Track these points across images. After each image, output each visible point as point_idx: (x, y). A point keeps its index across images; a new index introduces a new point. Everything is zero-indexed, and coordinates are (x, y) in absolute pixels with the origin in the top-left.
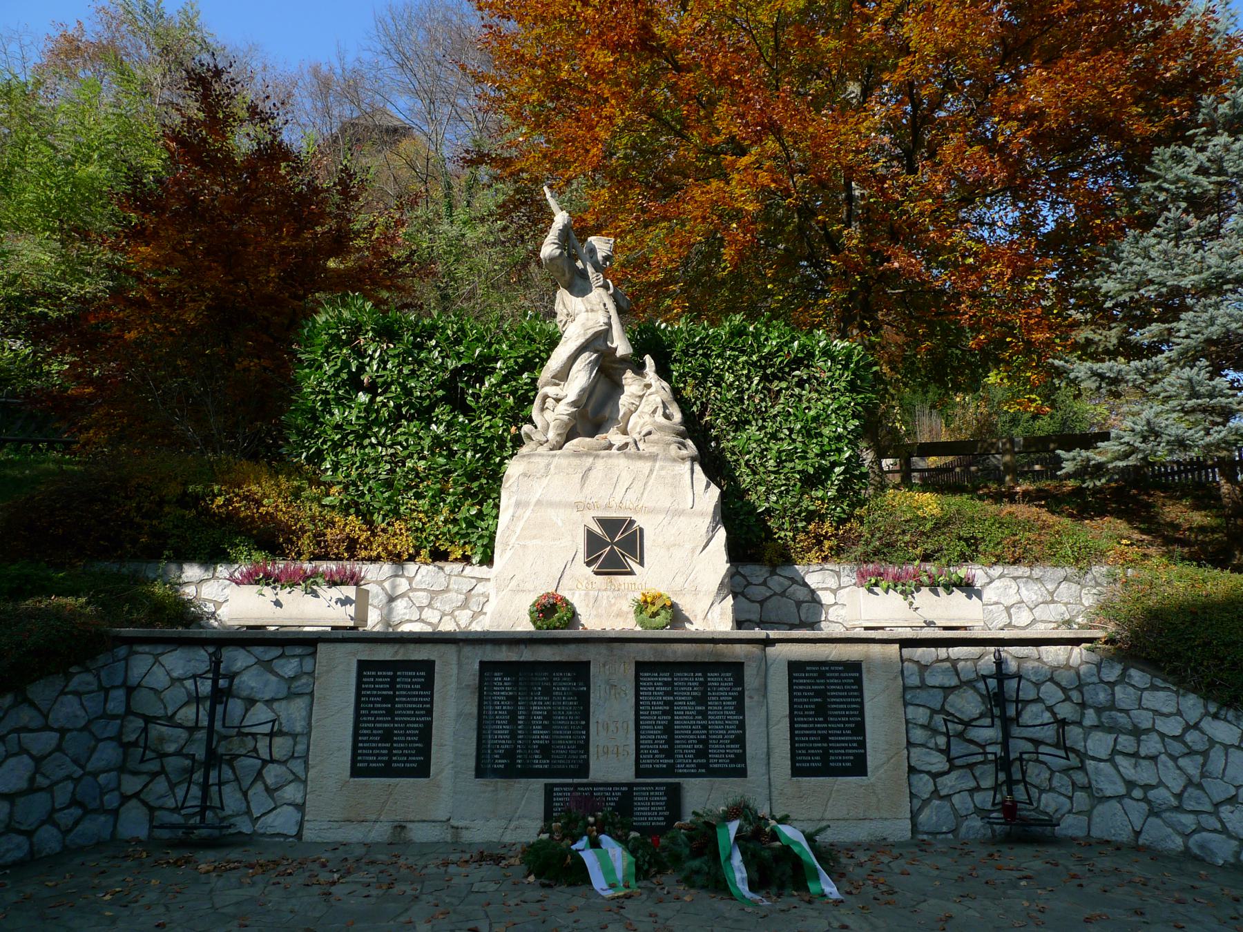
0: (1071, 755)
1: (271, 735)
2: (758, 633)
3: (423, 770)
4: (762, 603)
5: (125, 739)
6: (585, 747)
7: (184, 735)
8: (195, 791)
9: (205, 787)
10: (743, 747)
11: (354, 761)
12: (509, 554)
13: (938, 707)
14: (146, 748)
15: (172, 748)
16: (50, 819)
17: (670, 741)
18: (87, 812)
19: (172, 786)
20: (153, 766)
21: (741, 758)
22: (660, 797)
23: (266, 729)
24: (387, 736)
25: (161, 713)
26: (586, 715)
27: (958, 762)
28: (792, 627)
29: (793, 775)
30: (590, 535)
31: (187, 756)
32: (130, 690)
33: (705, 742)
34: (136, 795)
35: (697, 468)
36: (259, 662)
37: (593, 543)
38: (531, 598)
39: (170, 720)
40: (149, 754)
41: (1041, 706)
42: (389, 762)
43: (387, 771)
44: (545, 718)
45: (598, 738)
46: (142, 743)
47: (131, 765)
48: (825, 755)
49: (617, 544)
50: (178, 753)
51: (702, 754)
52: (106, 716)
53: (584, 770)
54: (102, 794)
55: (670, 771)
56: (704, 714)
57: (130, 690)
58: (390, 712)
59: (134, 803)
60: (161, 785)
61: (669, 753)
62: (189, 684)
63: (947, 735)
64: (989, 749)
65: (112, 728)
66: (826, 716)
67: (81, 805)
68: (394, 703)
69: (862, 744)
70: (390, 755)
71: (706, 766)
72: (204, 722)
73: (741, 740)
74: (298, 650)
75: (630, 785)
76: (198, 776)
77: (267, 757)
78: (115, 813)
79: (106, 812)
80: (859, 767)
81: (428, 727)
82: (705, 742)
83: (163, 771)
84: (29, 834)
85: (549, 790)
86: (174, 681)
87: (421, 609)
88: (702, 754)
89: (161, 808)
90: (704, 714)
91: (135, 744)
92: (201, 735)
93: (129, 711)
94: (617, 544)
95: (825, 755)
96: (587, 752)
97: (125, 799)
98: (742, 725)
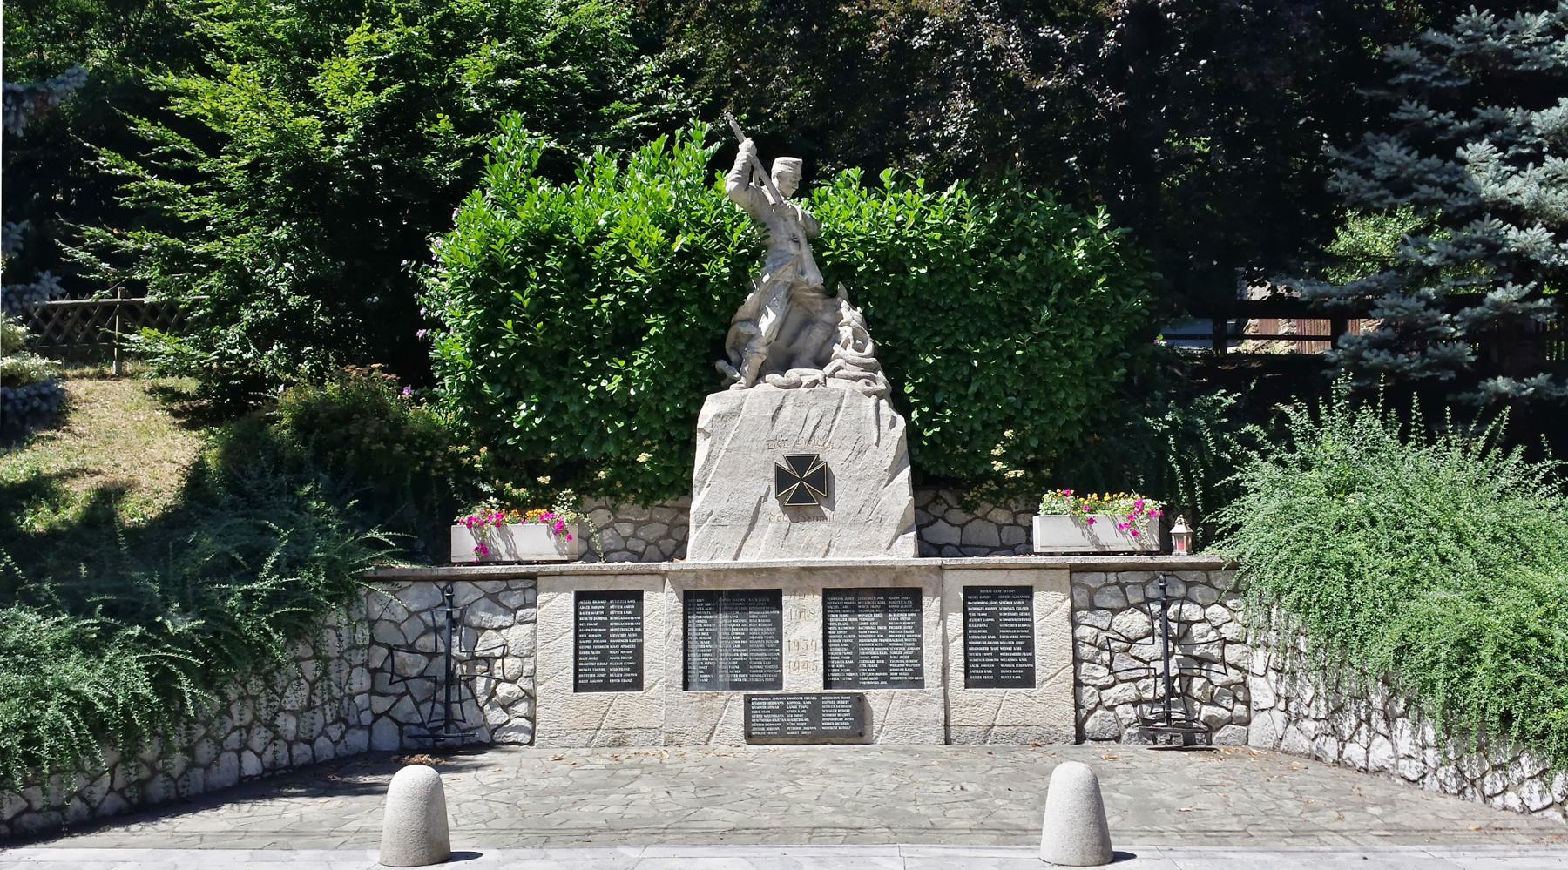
0: (1230, 670)
1: (503, 656)
2: (936, 561)
3: (637, 684)
4: (962, 526)
5: (372, 666)
6: (779, 663)
7: (424, 661)
8: (439, 708)
9: (447, 704)
10: (921, 662)
11: (576, 679)
12: (705, 491)
13: (1106, 626)
14: (393, 673)
15: (414, 672)
16: (323, 733)
17: (856, 657)
18: (349, 727)
19: (417, 704)
20: (400, 688)
21: (919, 672)
22: (846, 707)
23: (498, 652)
24: (604, 656)
25: (401, 642)
26: (779, 635)
27: (1122, 676)
28: (992, 550)
29: (967, 687)
30: (779, 470)
31: (428, 678)
32: (372, 623)
33: (886, 658)
34: (386, 713)
35: (883, 402)
36: (487, 595)
37: (782, 479)
38: (835, 470)
39: (411, 649)
40: (396, 678)
41: (1207, 626)
42: (608, 678)
43: (606, 686)
44: (743, 638)
45: (788, 657)
46: (388, 667)
47: (379, 688)
48: (997, 669)
49: (806, 480)
50: (421, 676)
51: (885, 667)
52: (354, 647)
53: (778, 683)
54: (359, 713)
55: (856, 683)
56: (886, 634)
57: (372, 623)
58: (606, 636)
59: (384, 720)
60: (407, 704)
61: (854, 668)
62: (427, 617)
63: (1111, 651)
64: (1152, 665)
65: (358, 658)
66: (998, 635)
67: (345, 721)
68: (608, 627)
69: (1031, 660)
70: (607, 672)
71: (887, 678)
72: (442, 649)
73: (918, 656)
74: (521, 584)
75: (820, 696)
76: (441, 695)
77: (500, 676)
78: (370, 728)
79: (362, 727)
80: (1028, 680)
81: (640, 647)
82: (886, 658)
83: (408, 692)
84: (311, 742)
85: (748, 701)
86: (411, 614)
87: (626, 539)
88: (881, 668)
89: (408, 724)
90: (886, 634)
91: (381, 670)
92: (441, 660)
93: (373, 641)
94: (806, 480)
95: (997, 669)
96: (781, 667)
97: (377, 717)
98: (919, 643)
